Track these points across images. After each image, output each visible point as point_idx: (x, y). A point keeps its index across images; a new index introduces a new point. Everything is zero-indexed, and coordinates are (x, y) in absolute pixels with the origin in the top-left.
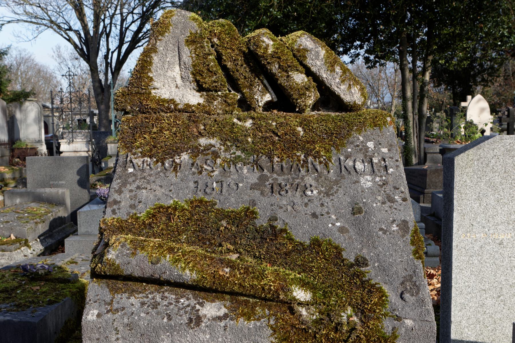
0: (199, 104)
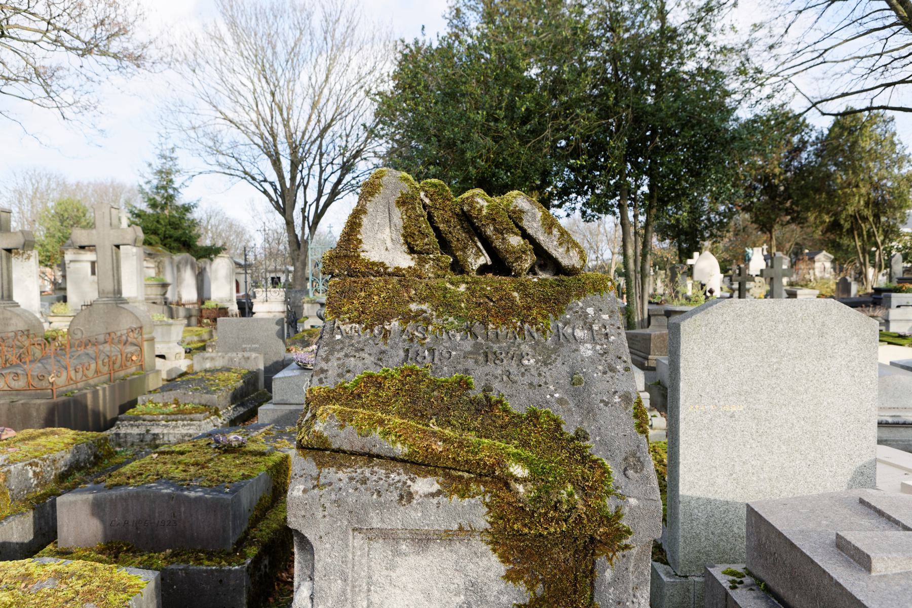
0: (410, 267)
